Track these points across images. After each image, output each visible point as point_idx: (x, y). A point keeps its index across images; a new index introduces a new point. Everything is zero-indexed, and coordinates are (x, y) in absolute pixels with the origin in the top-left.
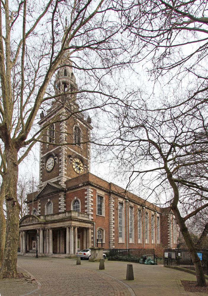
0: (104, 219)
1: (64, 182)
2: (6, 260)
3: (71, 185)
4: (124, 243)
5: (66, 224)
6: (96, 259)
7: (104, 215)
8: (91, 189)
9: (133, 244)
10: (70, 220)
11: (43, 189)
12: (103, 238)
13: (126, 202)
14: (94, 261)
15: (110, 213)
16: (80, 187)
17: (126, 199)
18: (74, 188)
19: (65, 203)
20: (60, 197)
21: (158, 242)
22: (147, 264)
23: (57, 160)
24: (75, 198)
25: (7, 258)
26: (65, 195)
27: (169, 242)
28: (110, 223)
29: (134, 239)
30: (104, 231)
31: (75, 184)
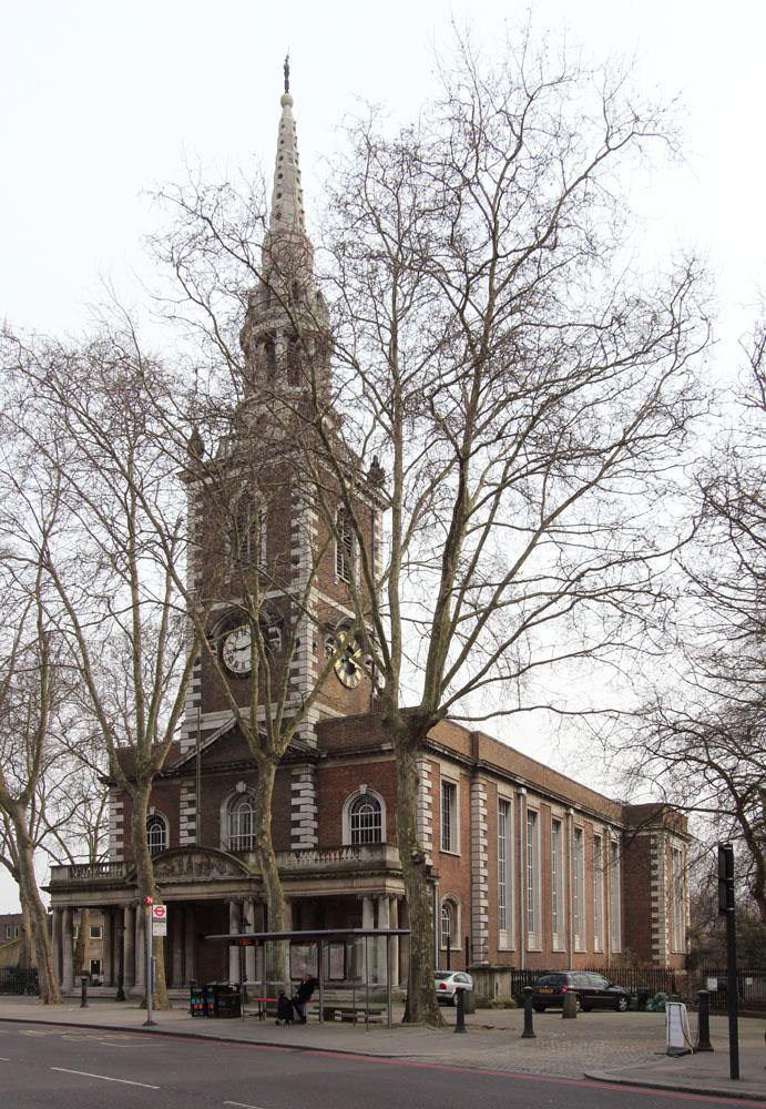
0: (459, 863)
1: (311, 728)
2: (424, 991)
3: (343, 739)
4: (541, 950)
5: (363, 886)
6: (494, 1000)
7: (457, 849)
8: (430, 762)
9: (562, 956)
10: (379, 875)
11: (210, 740)
12: (455, 932)
13: (519, 795)
14: (490, 1007)
15: (474, 841)
16: (382, 753)
17: (520, 786)
18: (356, 754)
19: (317, 801)
20: (297, 779)
21: (616, 946)
22: (654, 1011)
23: (279, 639)
24: (363, 789)
25: (425, 987)
26: (315, 773)
27: (654, 947)
28: (474, 878)
29: (540, 935)
30: (459, 907)
31: (366, 737)
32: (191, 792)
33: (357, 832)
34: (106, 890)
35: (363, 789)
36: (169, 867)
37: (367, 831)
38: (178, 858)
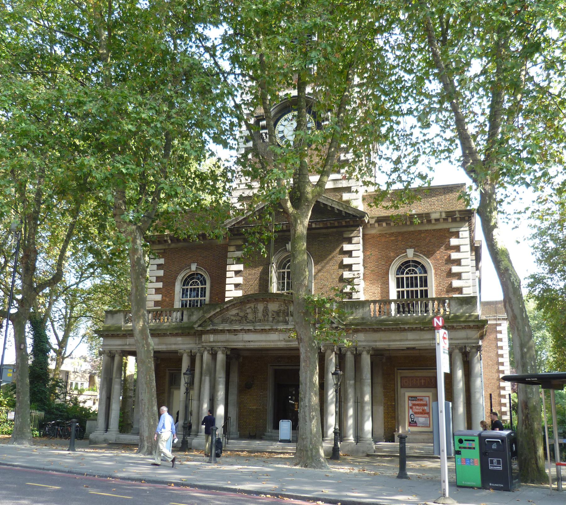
32: (238, 250)
33: (403, 292)
34: (165, 335)
35: (410, 253)
36: (242, 314)
37: (412, 291)
38: (252, 305)
